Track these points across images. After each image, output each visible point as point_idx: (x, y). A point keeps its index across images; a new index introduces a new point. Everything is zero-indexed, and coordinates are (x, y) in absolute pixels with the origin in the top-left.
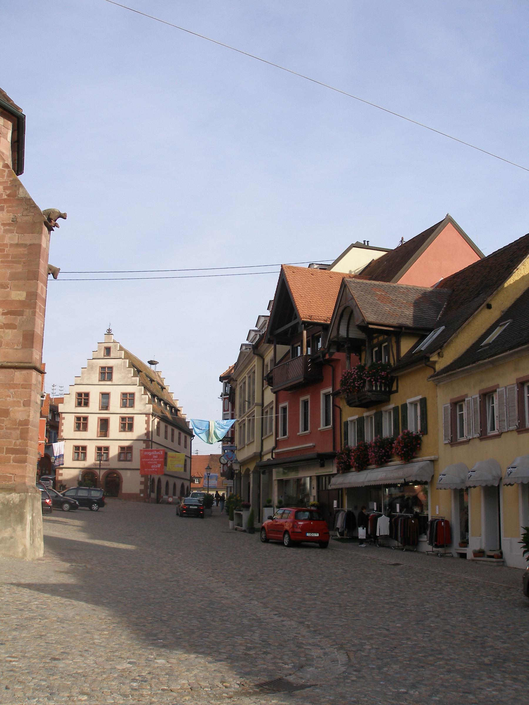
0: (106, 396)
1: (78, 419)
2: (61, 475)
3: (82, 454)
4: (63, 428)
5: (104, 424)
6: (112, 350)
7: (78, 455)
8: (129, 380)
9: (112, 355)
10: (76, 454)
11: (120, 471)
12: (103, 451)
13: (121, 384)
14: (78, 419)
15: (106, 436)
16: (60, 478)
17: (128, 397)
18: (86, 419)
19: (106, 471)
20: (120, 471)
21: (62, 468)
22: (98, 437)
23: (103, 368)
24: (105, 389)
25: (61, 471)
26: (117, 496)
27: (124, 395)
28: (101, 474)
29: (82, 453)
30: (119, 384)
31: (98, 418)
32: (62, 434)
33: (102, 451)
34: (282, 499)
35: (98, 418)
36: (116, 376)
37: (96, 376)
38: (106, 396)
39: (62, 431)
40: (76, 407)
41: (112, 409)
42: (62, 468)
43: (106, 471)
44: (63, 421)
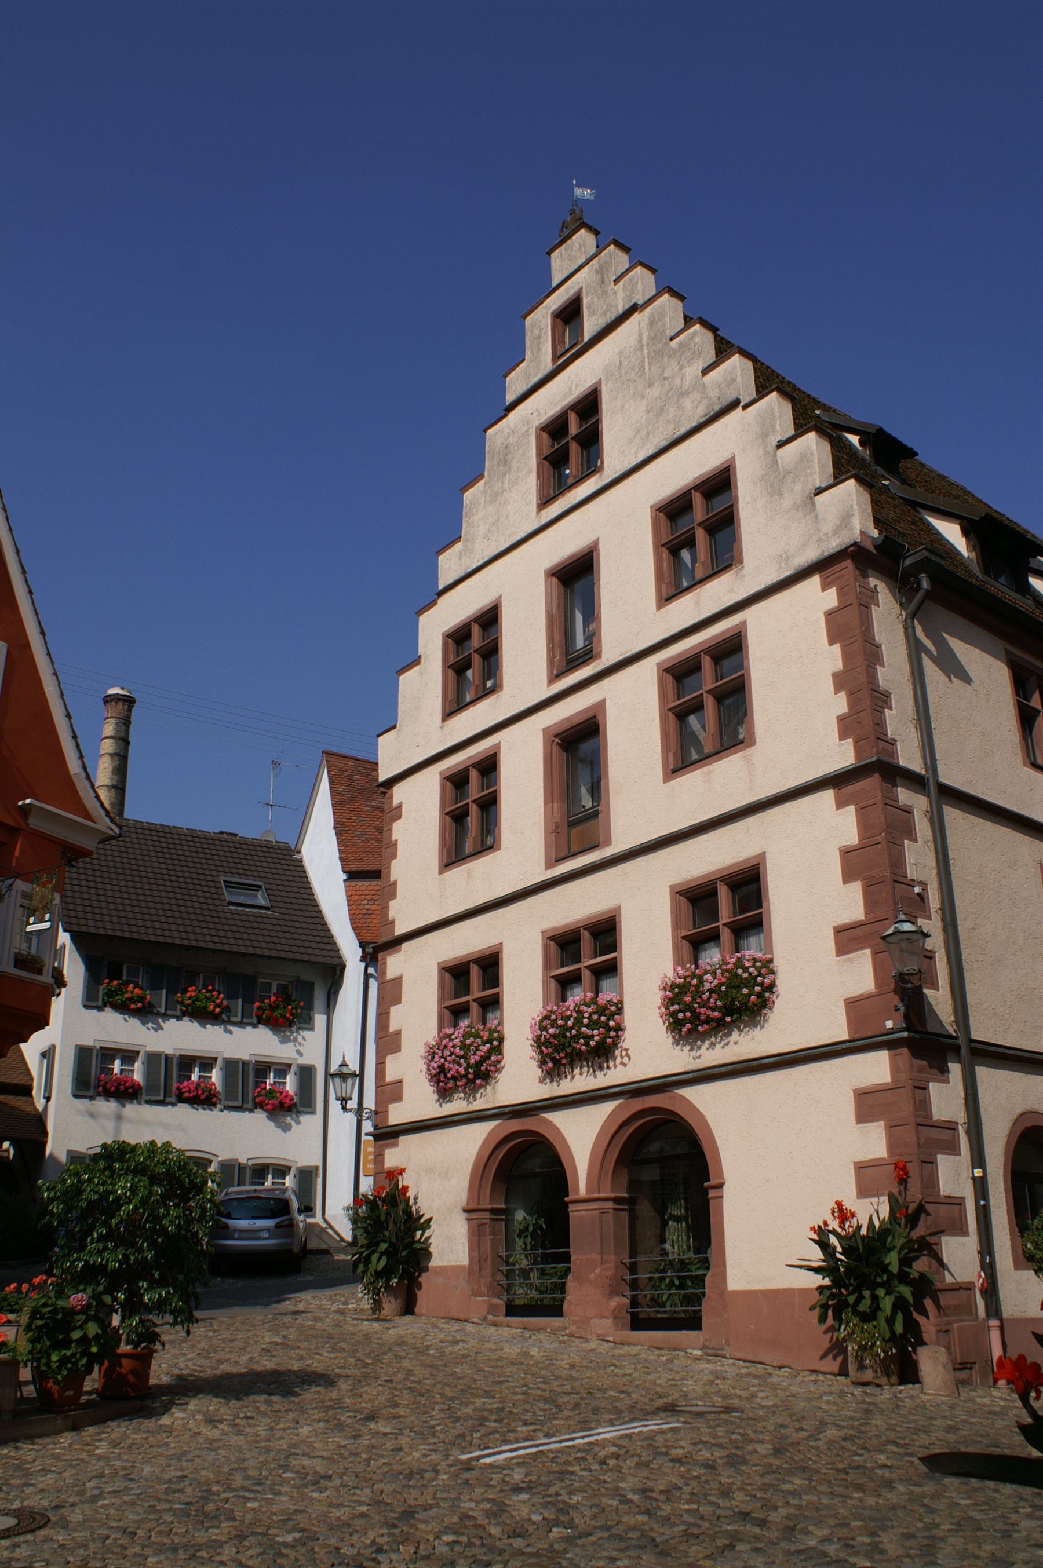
5: (579, 748)
38: (576, 576)
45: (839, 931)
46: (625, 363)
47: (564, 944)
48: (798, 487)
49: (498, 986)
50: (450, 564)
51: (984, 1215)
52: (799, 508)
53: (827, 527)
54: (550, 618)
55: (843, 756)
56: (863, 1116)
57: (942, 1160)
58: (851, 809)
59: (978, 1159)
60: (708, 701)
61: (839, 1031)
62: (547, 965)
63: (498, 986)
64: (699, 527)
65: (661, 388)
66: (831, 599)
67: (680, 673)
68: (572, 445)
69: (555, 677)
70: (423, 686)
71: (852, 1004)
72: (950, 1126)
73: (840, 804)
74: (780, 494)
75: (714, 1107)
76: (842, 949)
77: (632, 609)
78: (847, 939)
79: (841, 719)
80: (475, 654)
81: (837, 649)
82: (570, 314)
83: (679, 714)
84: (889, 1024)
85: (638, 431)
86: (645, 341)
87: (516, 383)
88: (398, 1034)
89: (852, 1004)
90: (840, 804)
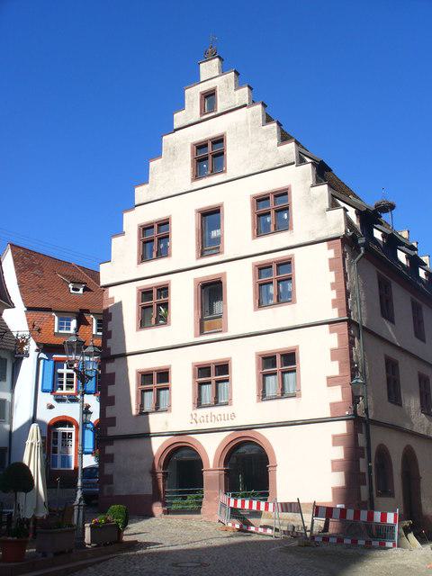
0: (211, 217)
5: (212, 292)
9: (221, 107)
24: (207, 199)
36: (235, 158)
38: (211, 217)
41: (229, 249)
45: (328, 378)
46: (239, 128)
47: (203, 370)
48: (319, 206)
49: (168, 381)
50: (141, 193)
51: (370, 477)
52: (317, 218)
53: (332, 225)
54: (197, 229)
55: (334, 314)
56: (334, 444)
57: (361, 460)
58: (336, 334)
59: (369, 461)
60: (275, 281)
61: (328, 414)
62: (138, 302)
63: (168, 381)
64: (272, 211)
65: (258, 154)
66: (331, 254)
67: (262, 269)
68: (209, 157)
69: (202, 114)
70: (125, 247)
71: (333, 405)
72: (362, 448)
73: (331, 332)
74: (311, 207)
75: (275, 441)
76: (329, 385)
77: (237, 229)
78: (331, 381)
79: (333, 301)
80: (155, 240)
81: (333, 273)
82: (209, 96)
83: (261, 287)
84: (347, 413)
85: (245, 161)
86: (249, 122)
87: (179, 118)
88: (333, 359)
89: (333, 405)
90: (331, 332)
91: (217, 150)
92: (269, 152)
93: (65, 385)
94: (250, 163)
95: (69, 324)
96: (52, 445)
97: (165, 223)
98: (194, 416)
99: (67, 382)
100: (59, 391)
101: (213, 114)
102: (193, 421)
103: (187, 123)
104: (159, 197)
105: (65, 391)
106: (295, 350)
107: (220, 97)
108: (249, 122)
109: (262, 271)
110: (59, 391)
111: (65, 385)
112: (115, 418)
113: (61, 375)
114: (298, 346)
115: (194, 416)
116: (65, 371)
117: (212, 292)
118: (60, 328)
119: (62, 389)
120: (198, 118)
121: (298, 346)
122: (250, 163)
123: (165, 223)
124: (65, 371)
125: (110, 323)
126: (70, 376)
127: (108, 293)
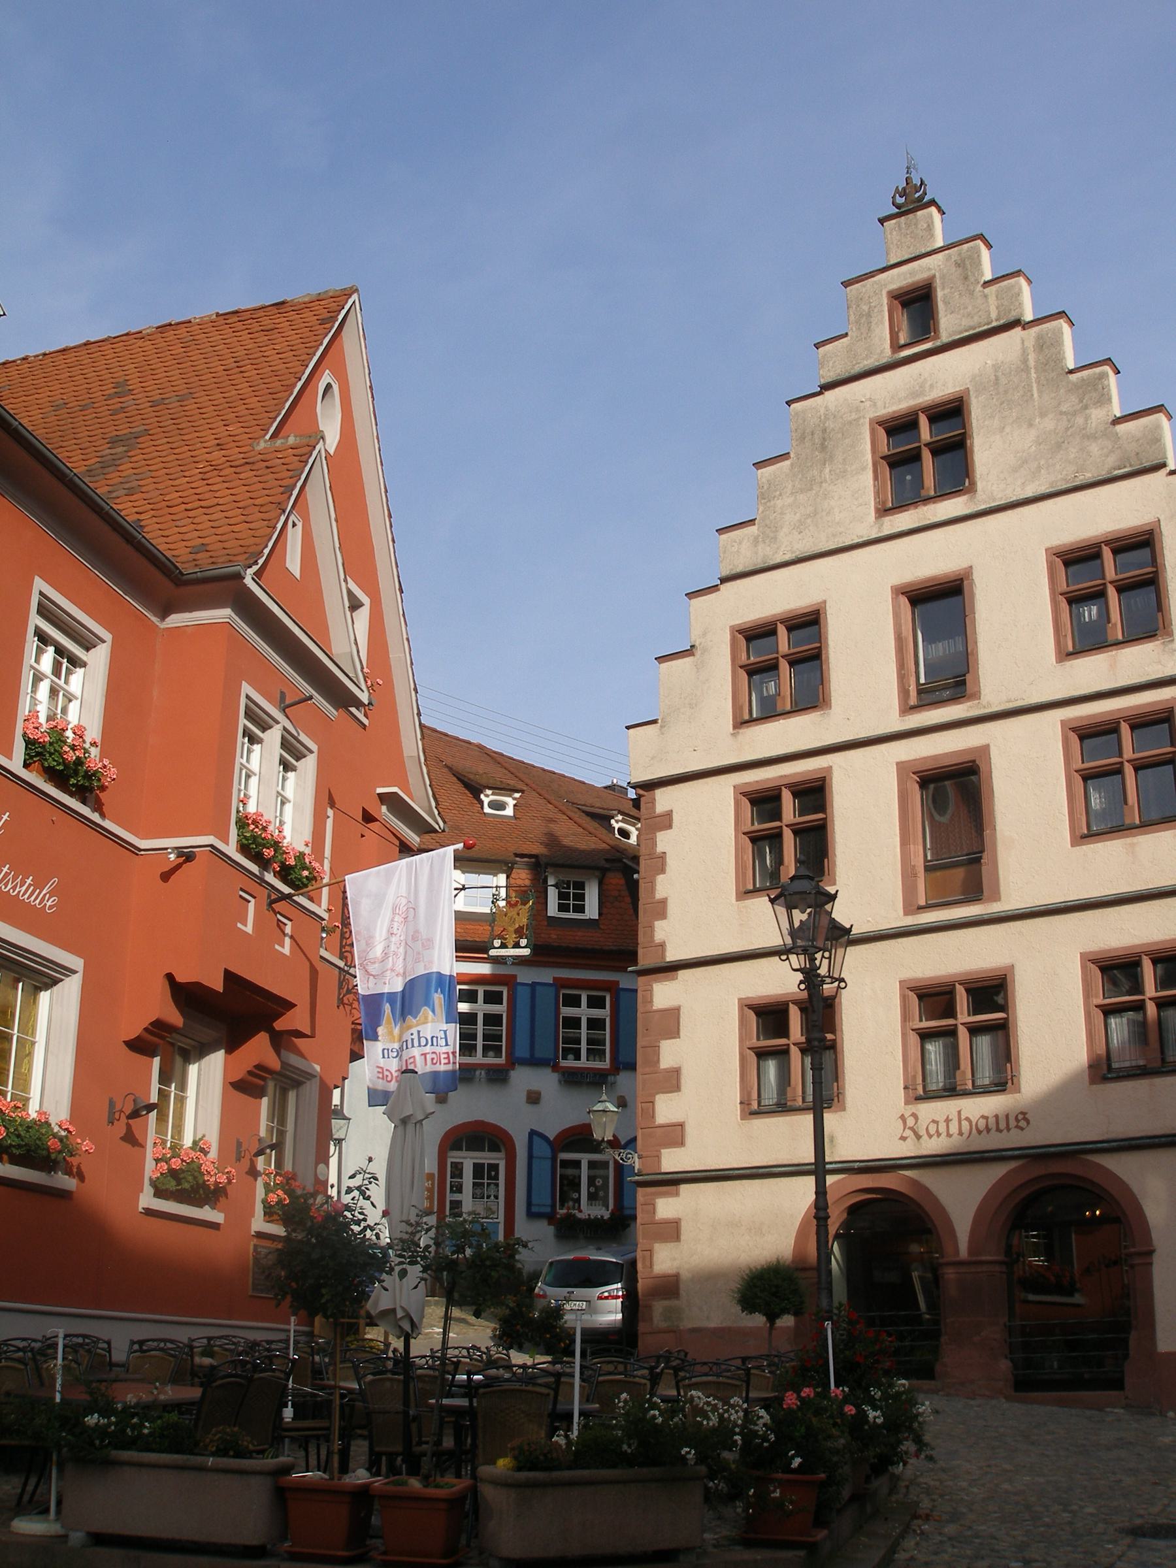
0: (939, 604)
1: (764, 802)
2: (672, 1231)
3: (984, 1042)
4: (665, 886)
5: (953, 798)
6: (940, 294)
7: (952, 1061)
8: (1094, 448)
9: (948, 324)
10: (934, 1049)
11: (1121, 1166)
12: (964, 1016)
13: (1044, 489)
14: (764, 802)
15: (974, 891)
16: (664, 1260)
17: (1110, 573)
18: (814, 793)
19: (998, 1171)
20: (1121, 1166)
21: (674, 1181)
22: (911, 908)
23: (899, 426)
24: (929, 558)
25: (666, 1207)
26: (1116, 1384)
27: (1076, 559)
28: (961, 1201)
29: (975, 1030)
30: (1029, 493)
31: (901, 767)
32: (662, 930)
33: (965, 1017)
34: (178, 1060)
35: (901, 767)
36: (993, 454)
37: (856, 488)
38: (939, 604)
39: (661, 909)
40: (825, 602)
41: (996, 682)
42: (674, 1181)
43: (998, 1171)
44: (664, 841)
46: (1003, 381)
86: (1032, 363)
91: (948, 433)
92: (1092, 437)
93: (584, 1046)
94: (1039, 468)
95: (581, 897)
96: (449, 1197)
97: (809, 623)
98: (911, 1122)
99: (590, 1042)
100: (570, 1063)
101: (927, 346)
102: (908, 1133)
103: (857, 369)
104: (788, 557)
105: (583, 1063)
106: (962, 580)
107: (946, 303)
108: (1032, 363)
109: (1086, 741)
110: (570, 1063)
111: (584, 1046)
112: (681, 1125)
113: (574, 1023)
114: (969, 571)
115: (911, 1122)
116: (584, 1012)
117: (953, 798)
118: (562, 908)
119: (578, 1058)
120: (886, 354)
121: (969, 571)
122: (1039, 468)
123: (809, 623)
124: (584, 1012)
125: (660, 878)
126: (595, 1024)
127: (653, 801)
